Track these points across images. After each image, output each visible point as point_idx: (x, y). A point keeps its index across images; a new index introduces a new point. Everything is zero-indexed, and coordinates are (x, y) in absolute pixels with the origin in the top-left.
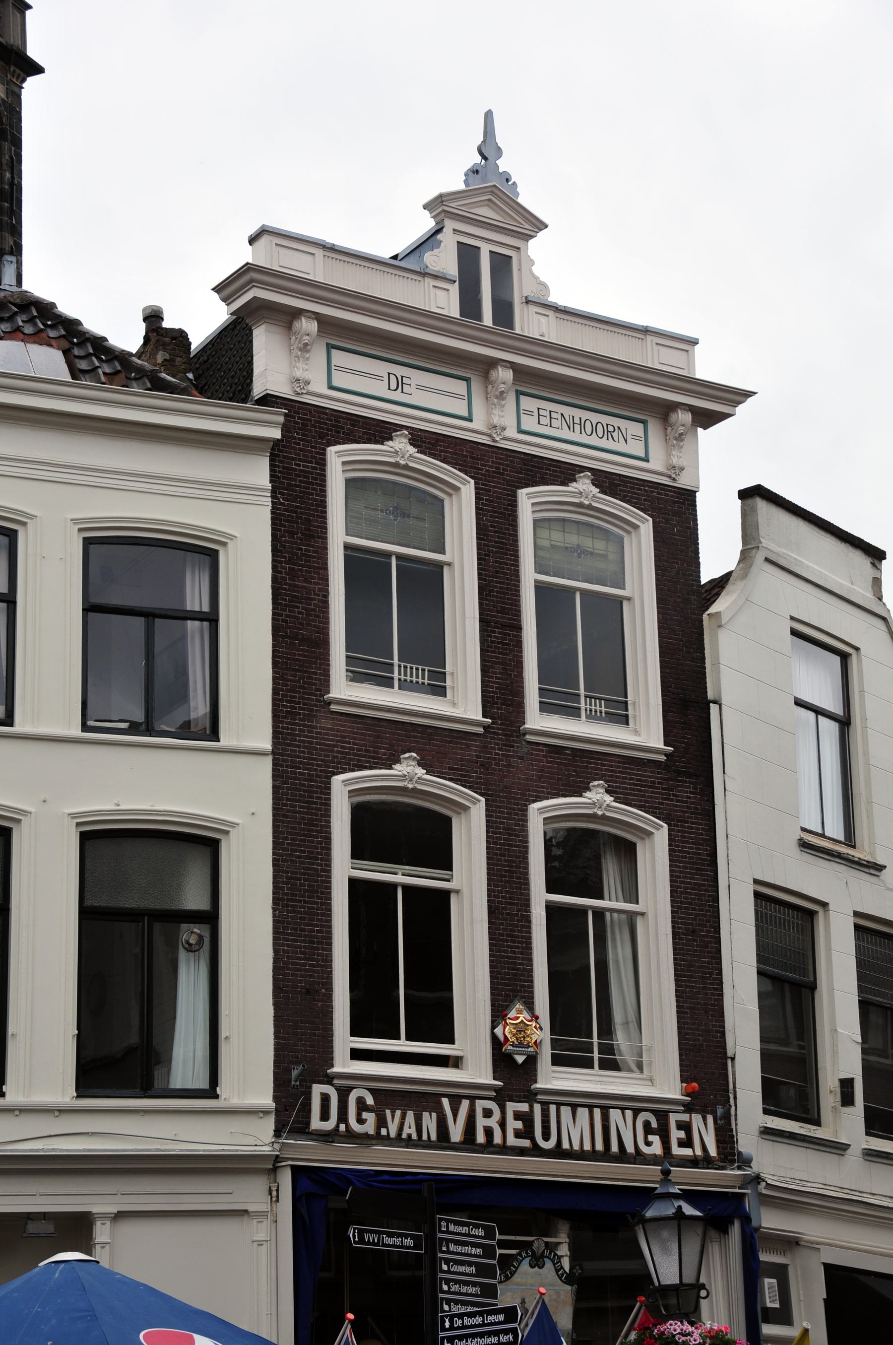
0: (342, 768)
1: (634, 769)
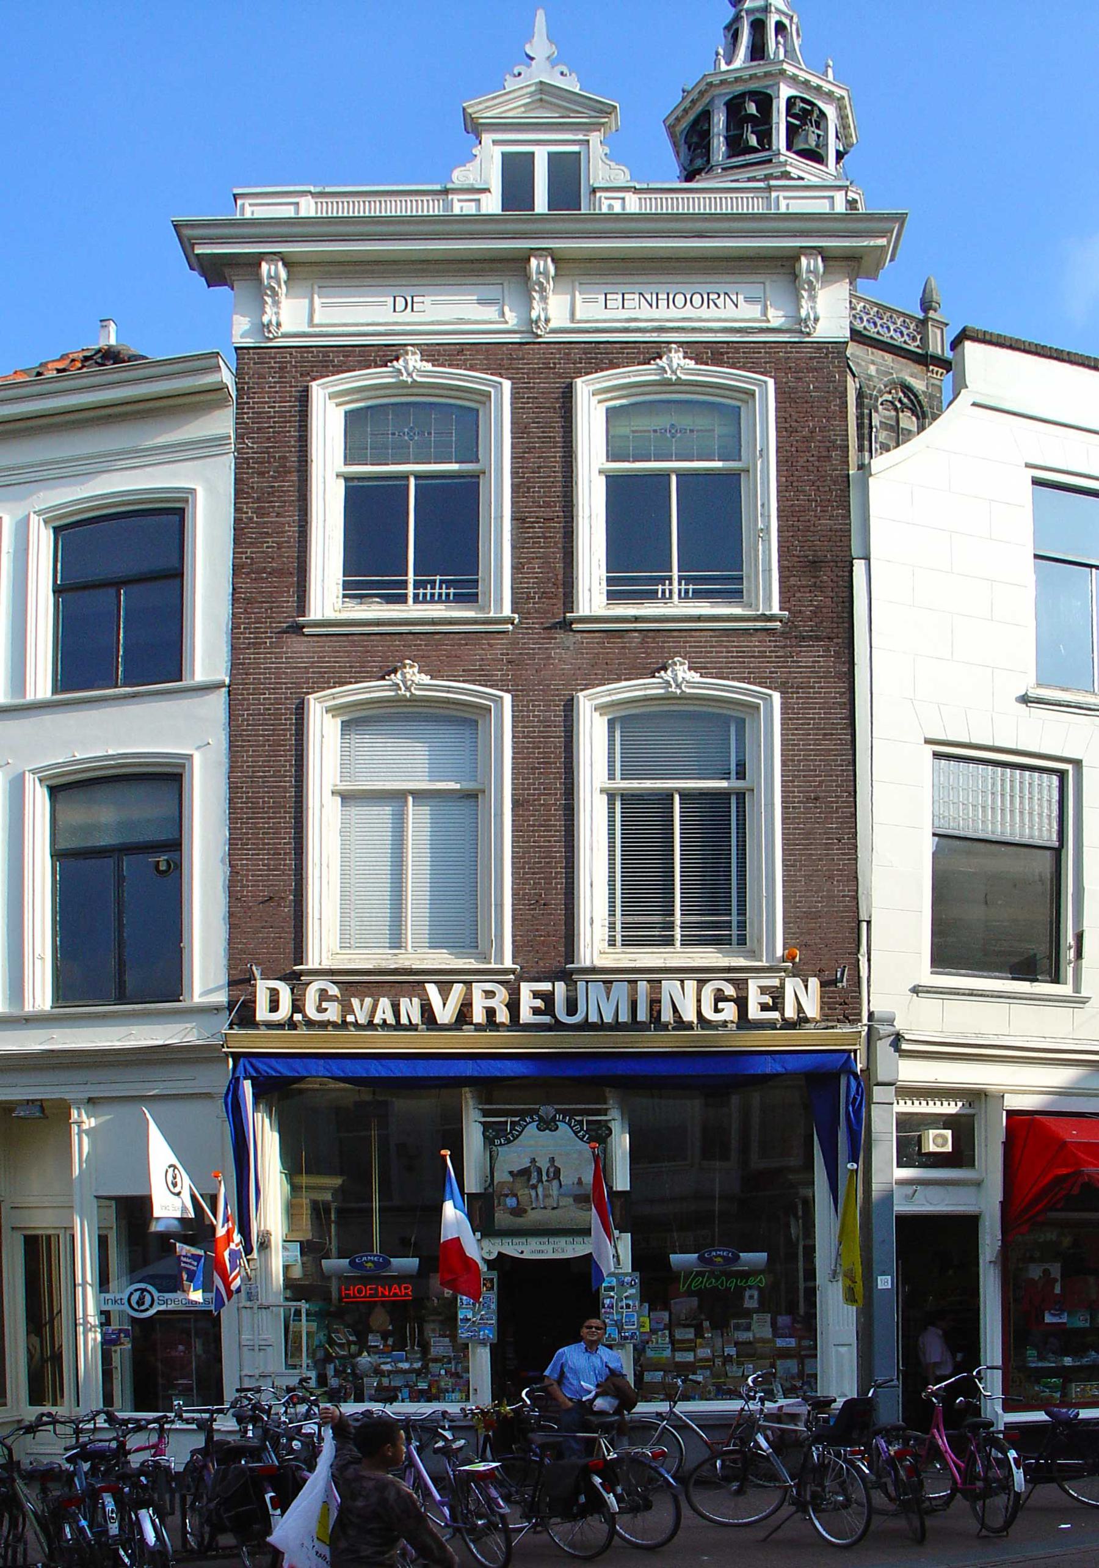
0: (318, 687)
1: (734, 642)
